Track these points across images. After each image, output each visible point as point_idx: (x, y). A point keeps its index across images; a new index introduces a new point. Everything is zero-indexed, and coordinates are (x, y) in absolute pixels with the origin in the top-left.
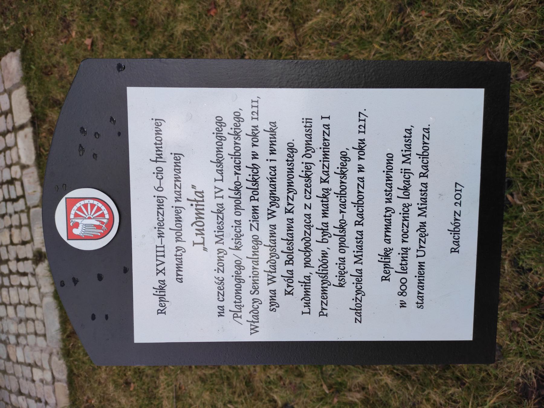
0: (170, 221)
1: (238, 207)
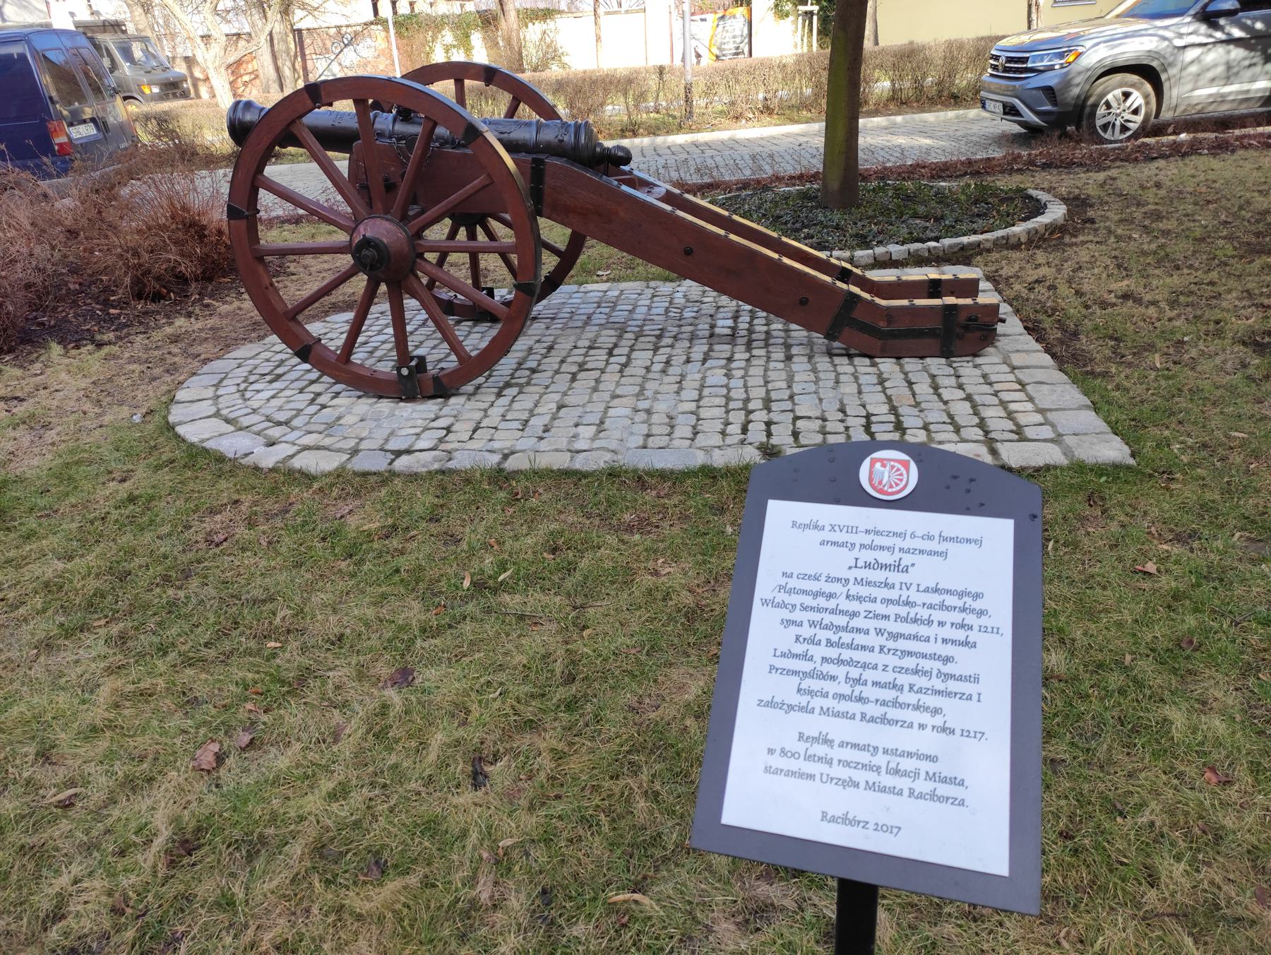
0: (879, 541)
1: (889, 602)
